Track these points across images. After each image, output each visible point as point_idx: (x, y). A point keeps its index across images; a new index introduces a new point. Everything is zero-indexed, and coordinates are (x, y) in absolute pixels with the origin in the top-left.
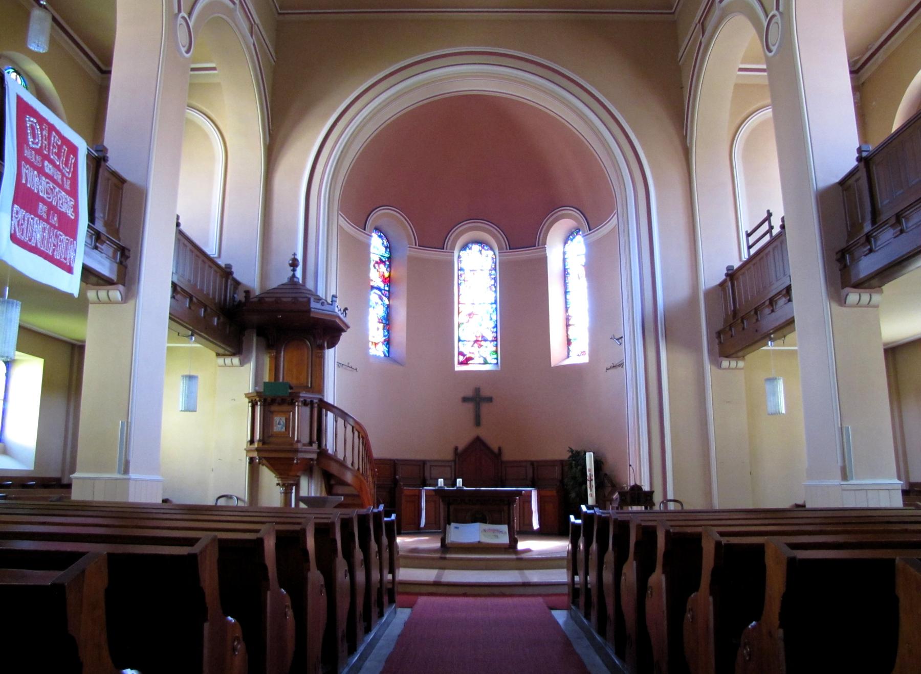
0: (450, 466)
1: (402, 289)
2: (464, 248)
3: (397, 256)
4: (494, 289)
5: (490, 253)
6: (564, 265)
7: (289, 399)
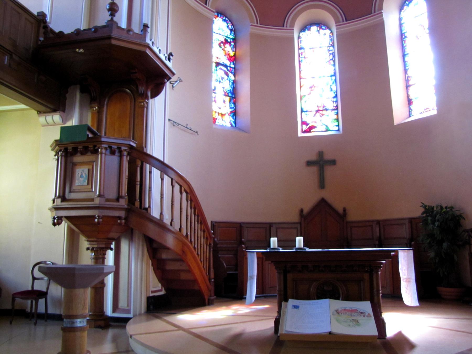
0: (297, 228)
1: (245, 65)
2: (303, 29)
3: (241, 37)
4: (332, 63)
5: (328, 32)
6: (401, 31)
7: (91, 146)
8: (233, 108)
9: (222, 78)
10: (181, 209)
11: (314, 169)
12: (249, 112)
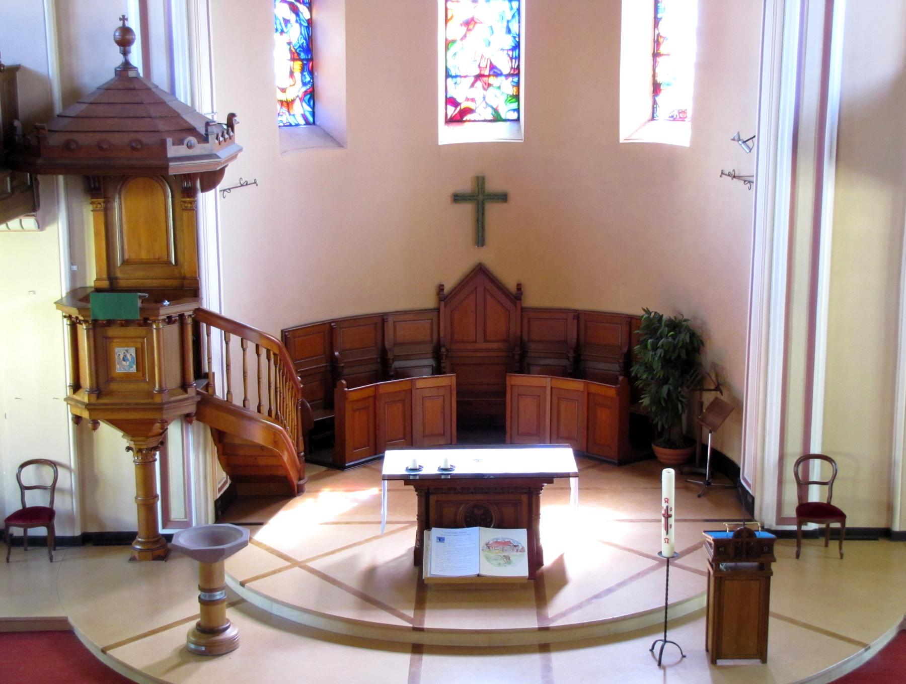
8: (309, 82)
9: (287, 22)
10: (259, 378)
11: (468, 208)
12: (344, 102)
